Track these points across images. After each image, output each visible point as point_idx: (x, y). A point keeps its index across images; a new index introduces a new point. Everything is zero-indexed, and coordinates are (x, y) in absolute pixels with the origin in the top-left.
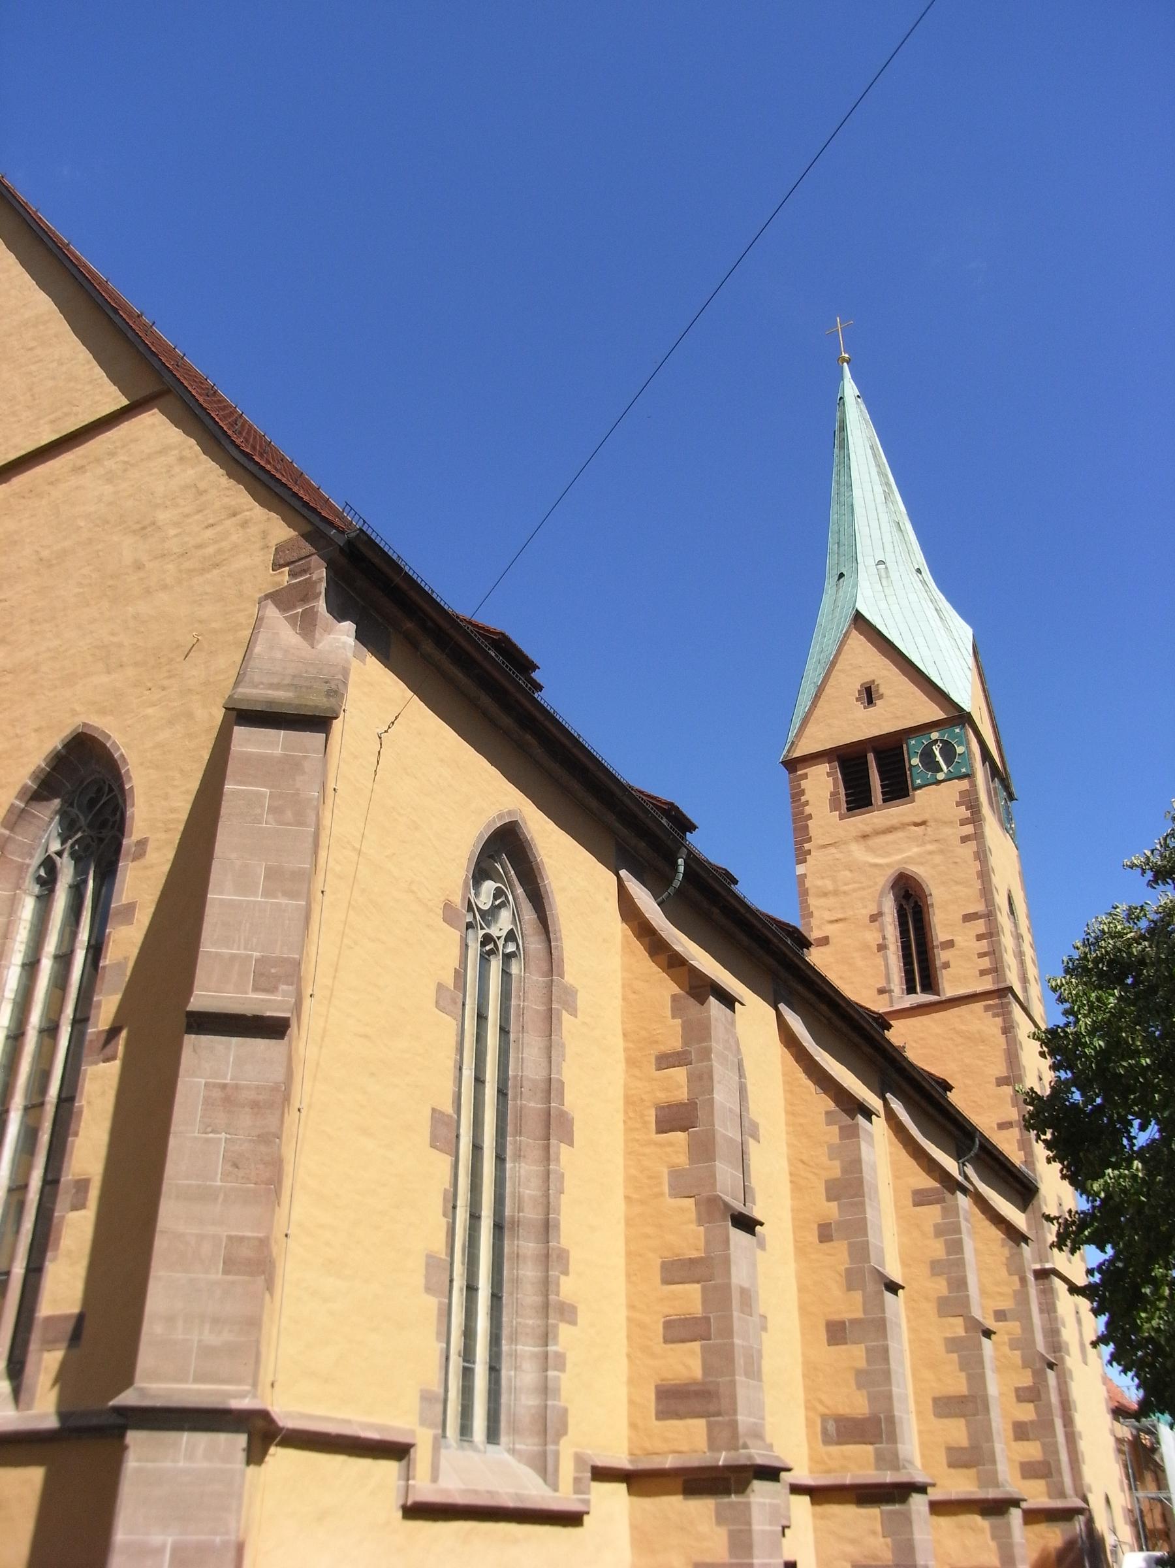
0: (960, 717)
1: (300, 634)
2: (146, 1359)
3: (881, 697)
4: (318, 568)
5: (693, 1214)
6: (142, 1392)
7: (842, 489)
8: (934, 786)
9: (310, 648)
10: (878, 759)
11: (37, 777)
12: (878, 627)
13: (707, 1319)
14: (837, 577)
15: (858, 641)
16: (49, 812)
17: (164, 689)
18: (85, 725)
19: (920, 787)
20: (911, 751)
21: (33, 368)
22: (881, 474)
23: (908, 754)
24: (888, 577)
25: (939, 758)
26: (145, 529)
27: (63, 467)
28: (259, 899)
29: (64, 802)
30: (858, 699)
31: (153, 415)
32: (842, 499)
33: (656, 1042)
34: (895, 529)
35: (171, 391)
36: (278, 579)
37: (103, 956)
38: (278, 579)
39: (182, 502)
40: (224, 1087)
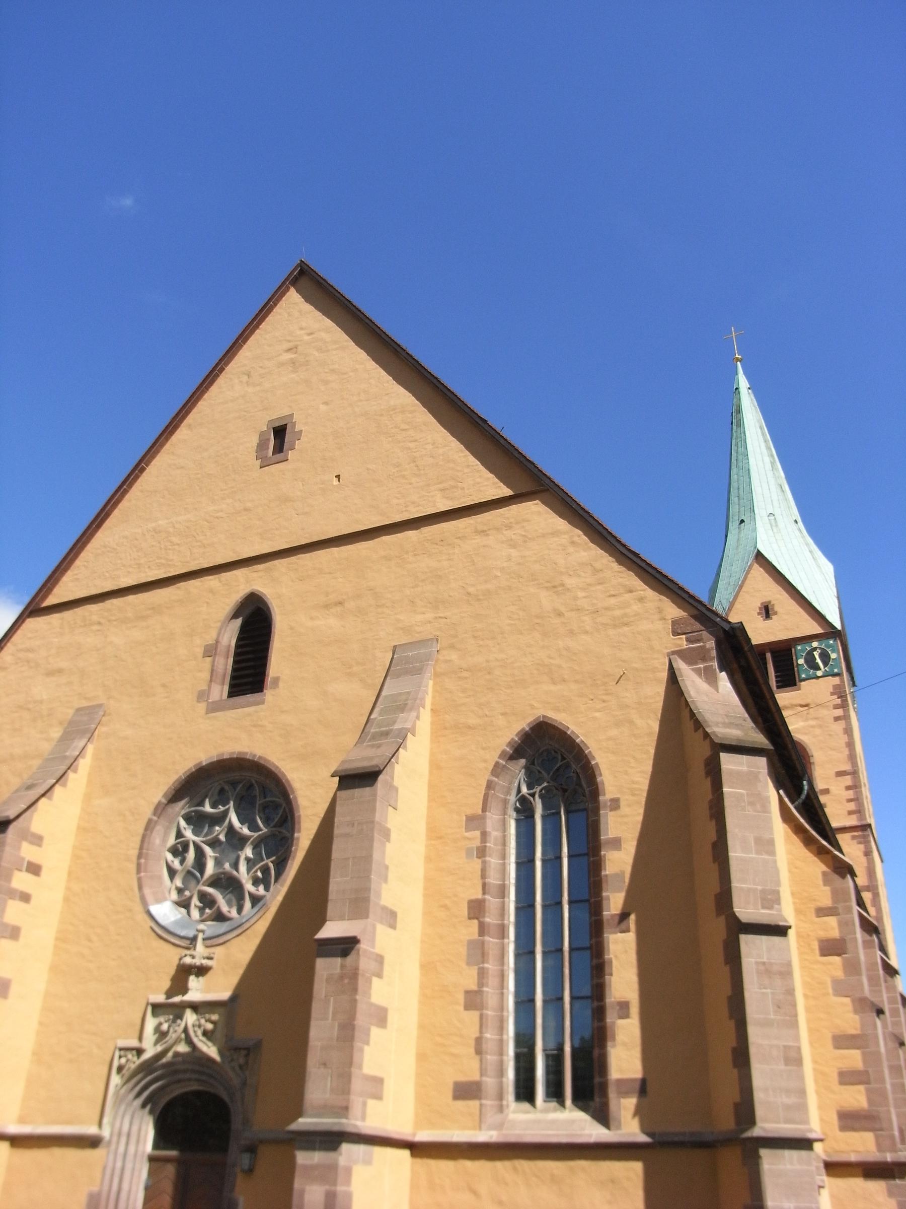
0: (833, 632)
1: (705, 681)
2: (759, 1112)
3: (776, 613)
4: (709, 640)
5: (850, 1007)
6: (763, 1129)
7: (740, 457)
8: (814, 680)
9: (716, 692)
10: (773, 657)
11: (513, 746)
12: (774, 563)
13: (867, 1072)
14: (738, 522)
15: (758, 572)
16: (518, 768)
17: (604, 701)
18: (544, 716)
19: (804, 680)
20: (798, 655)
21: (412, 445)
22: (768, 448)
23: (796, 655)
24: (777, 526)
25: (818, 661)
26: (556, 588)
27: (466, 528)
28: (754, 856)
29: (528, 761)
30: (759, 614)
31: (536, 504)
32: (740, 464)
33: (815, 900)
34: (779, 490)
35: (549, 490)
36: (679, 642)
37: (603, 868)
38: (679, 642)
39: (582, 574)
40: (764, 963)
